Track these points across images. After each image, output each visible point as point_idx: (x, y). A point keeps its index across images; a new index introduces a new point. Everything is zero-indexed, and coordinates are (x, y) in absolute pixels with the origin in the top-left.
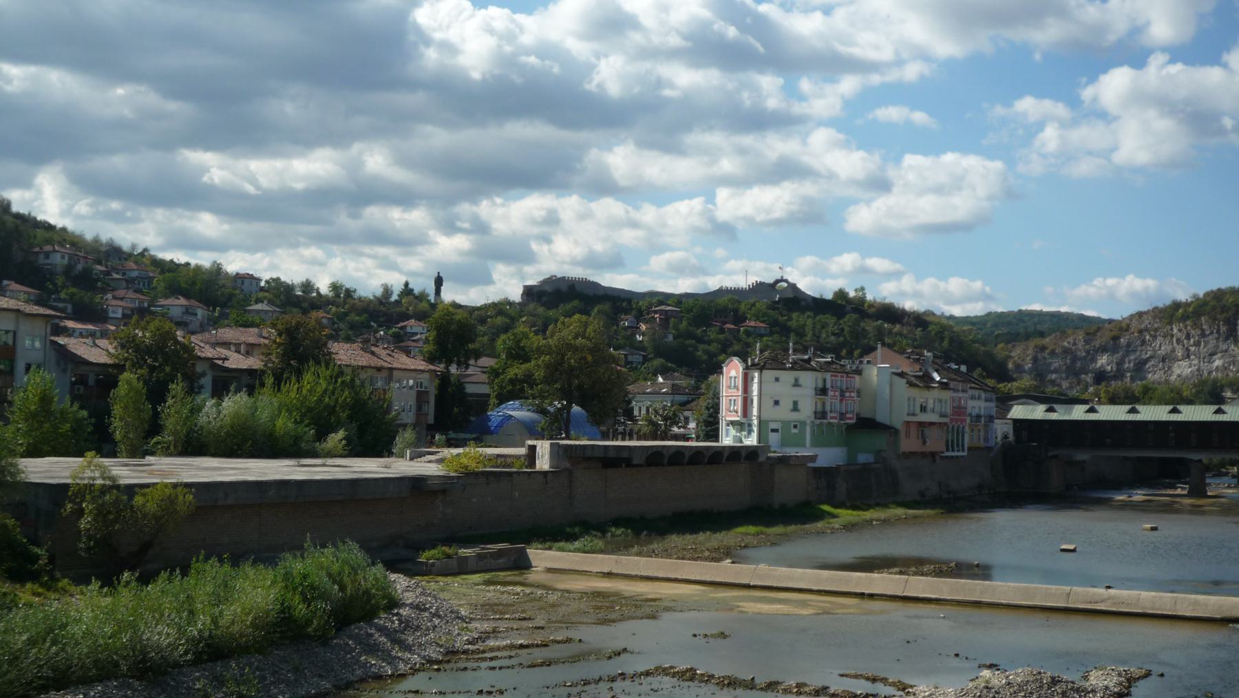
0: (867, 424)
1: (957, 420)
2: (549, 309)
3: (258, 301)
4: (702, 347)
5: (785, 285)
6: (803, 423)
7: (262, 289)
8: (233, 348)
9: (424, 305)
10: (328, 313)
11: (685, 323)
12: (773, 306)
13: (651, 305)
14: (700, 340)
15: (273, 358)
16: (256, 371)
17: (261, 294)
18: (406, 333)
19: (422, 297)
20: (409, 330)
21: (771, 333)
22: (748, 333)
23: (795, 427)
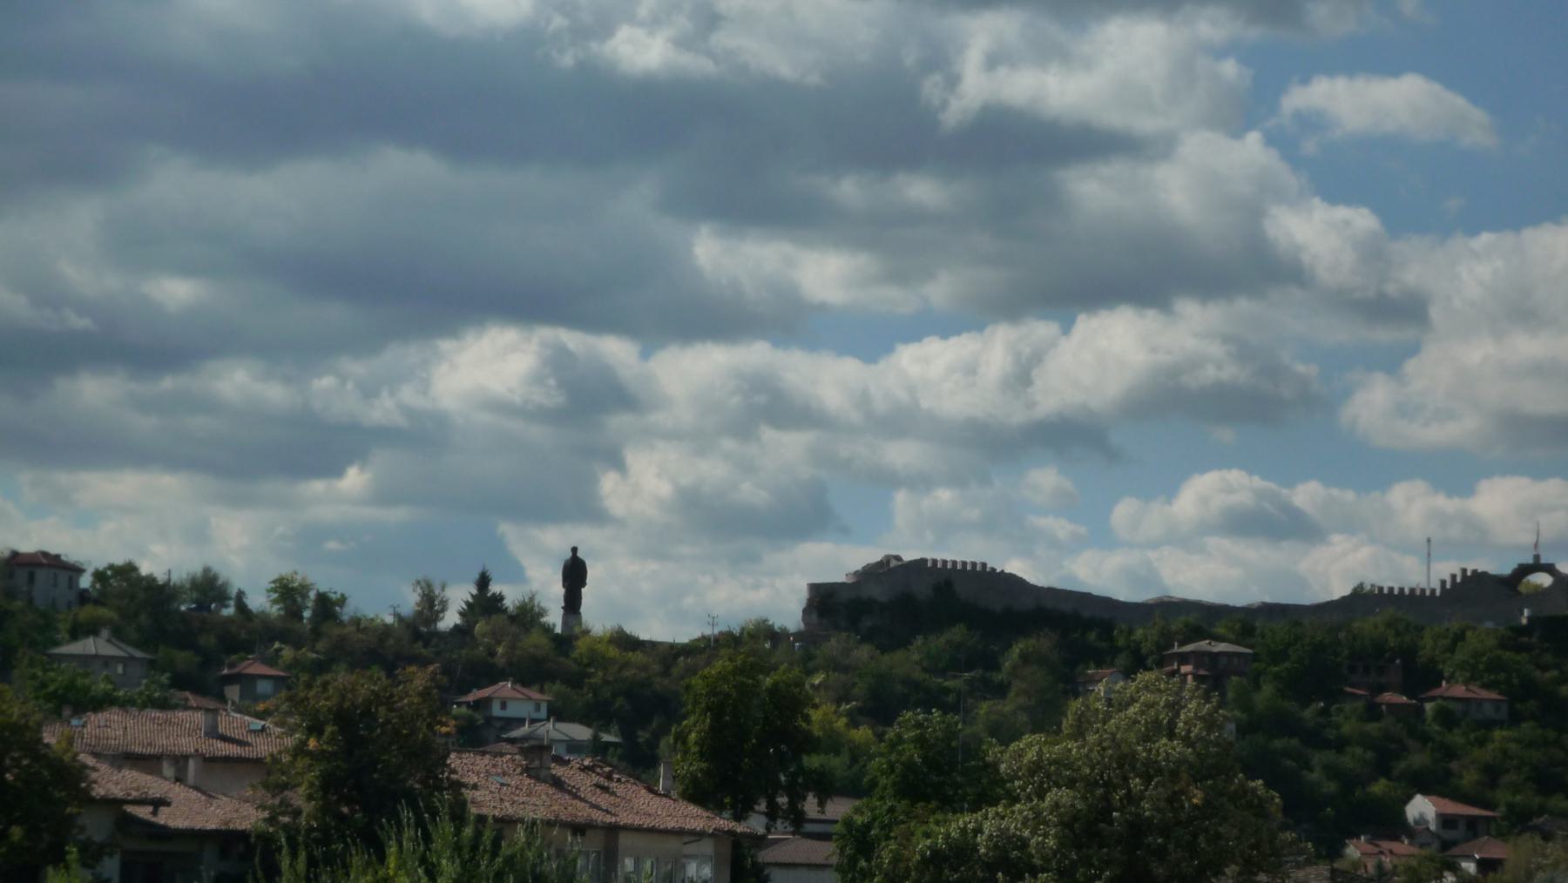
2: (884, 649)
3: (78, 631)
4: (1319, 758)
5: (1544, 580)
7: (83, 597)
8: (168, 770)
9: (534, 642)
10: (272, 661)
11: (1268, 689)
12: (1515, 638)
13: (1167, 639)
14: (1315, 739)
15: (298, 797)
16: (242, 836)
17: (86, 613)
18: (490, 720)
19: (528, 616)
20: (496, 710)
21: (1515, 719)
22: (1447, 718)
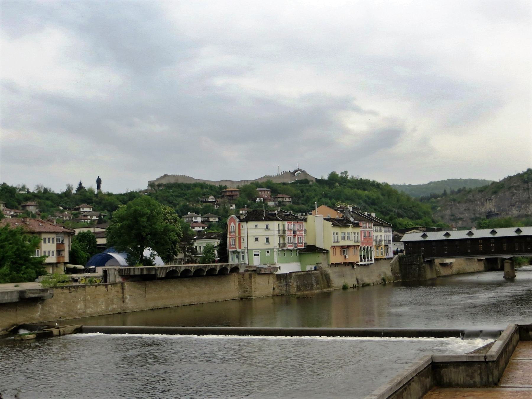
0: (311, 249)
1: (366, 244)
6: (272, 250)
19: (91, 191)
23: (268, 252)
